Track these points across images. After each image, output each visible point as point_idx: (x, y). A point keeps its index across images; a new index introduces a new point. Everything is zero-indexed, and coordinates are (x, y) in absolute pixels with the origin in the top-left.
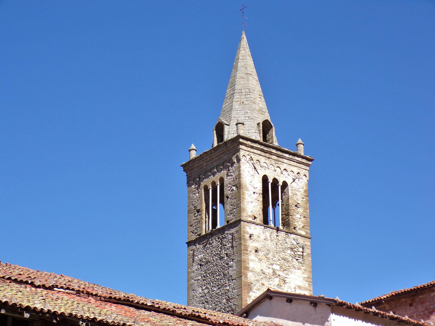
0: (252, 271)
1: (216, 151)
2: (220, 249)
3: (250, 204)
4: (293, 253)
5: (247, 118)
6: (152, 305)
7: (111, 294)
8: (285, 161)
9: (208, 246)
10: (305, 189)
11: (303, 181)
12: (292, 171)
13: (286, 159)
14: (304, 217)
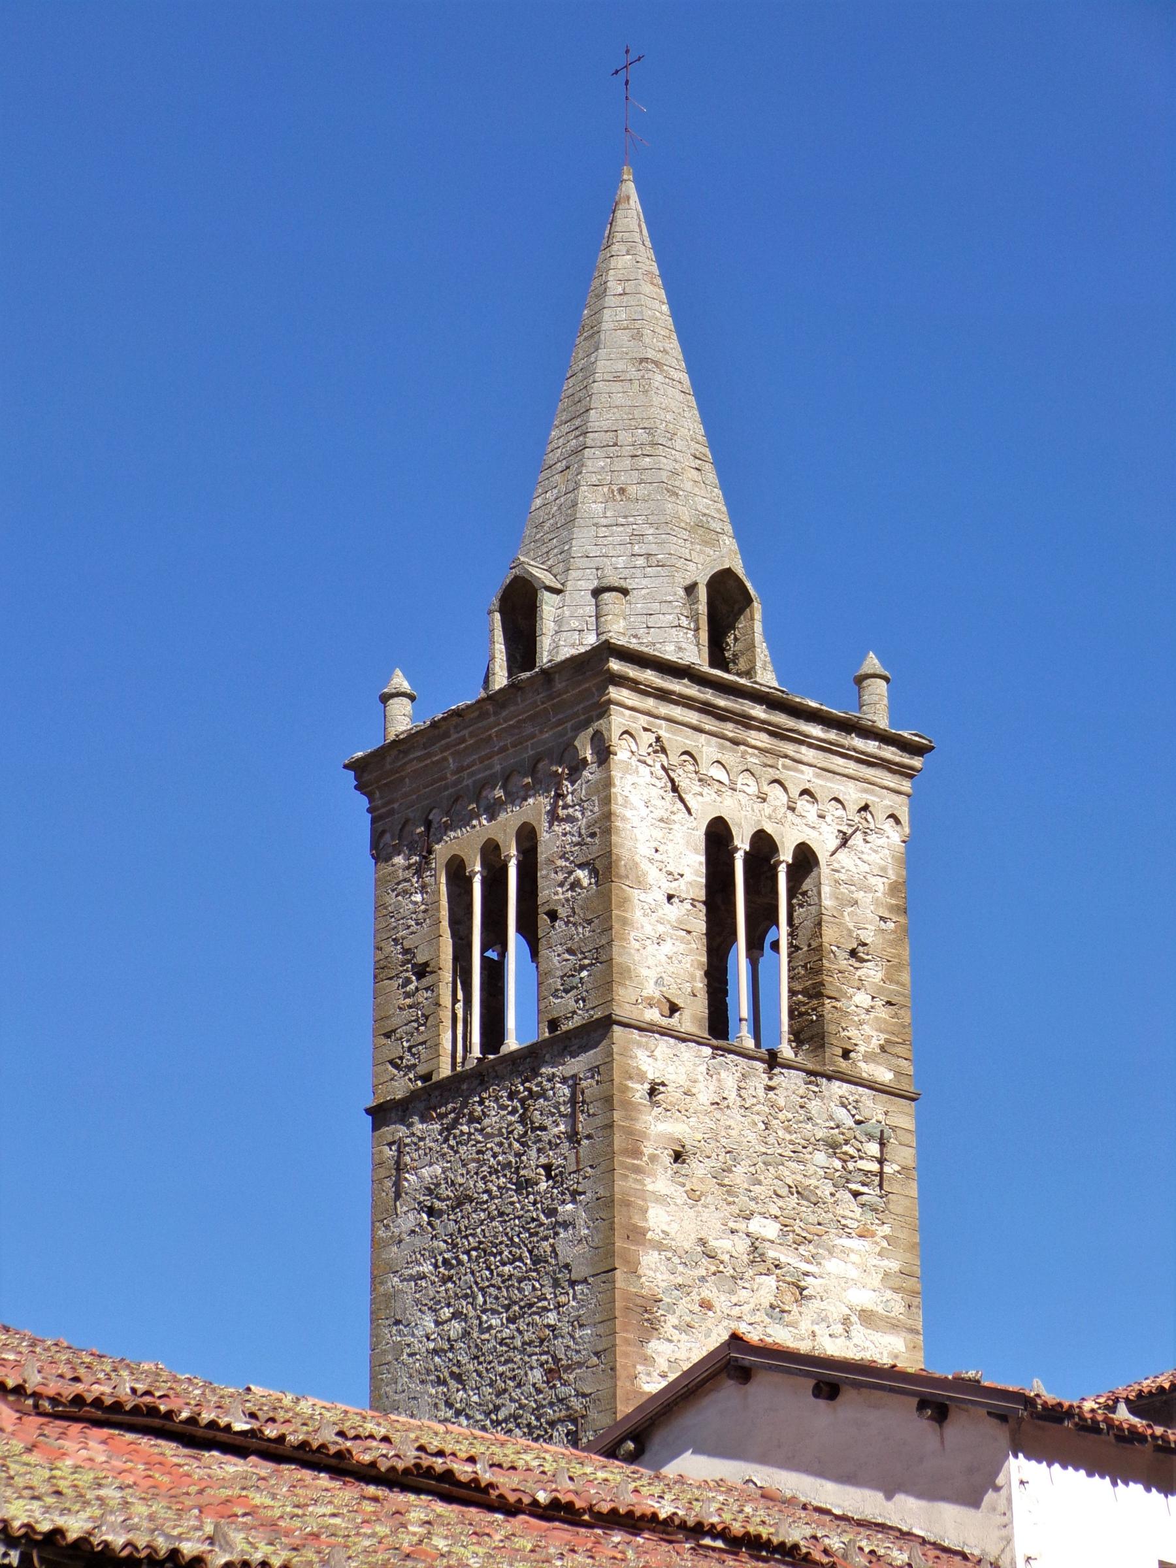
0: (659, 1247)
1: (503, 706)
2: (516, 1145)
3: (651, 948)
4: (838, 1164)
5: (641, 561)
6: (252, 1431)
7: (77, 1379)
8: (808, 754)
9: (465, 1128)
10: (894, 878)
11: (882, 841)
12: (836, 800)
13: (810, 746)
14: (889, 1003)
